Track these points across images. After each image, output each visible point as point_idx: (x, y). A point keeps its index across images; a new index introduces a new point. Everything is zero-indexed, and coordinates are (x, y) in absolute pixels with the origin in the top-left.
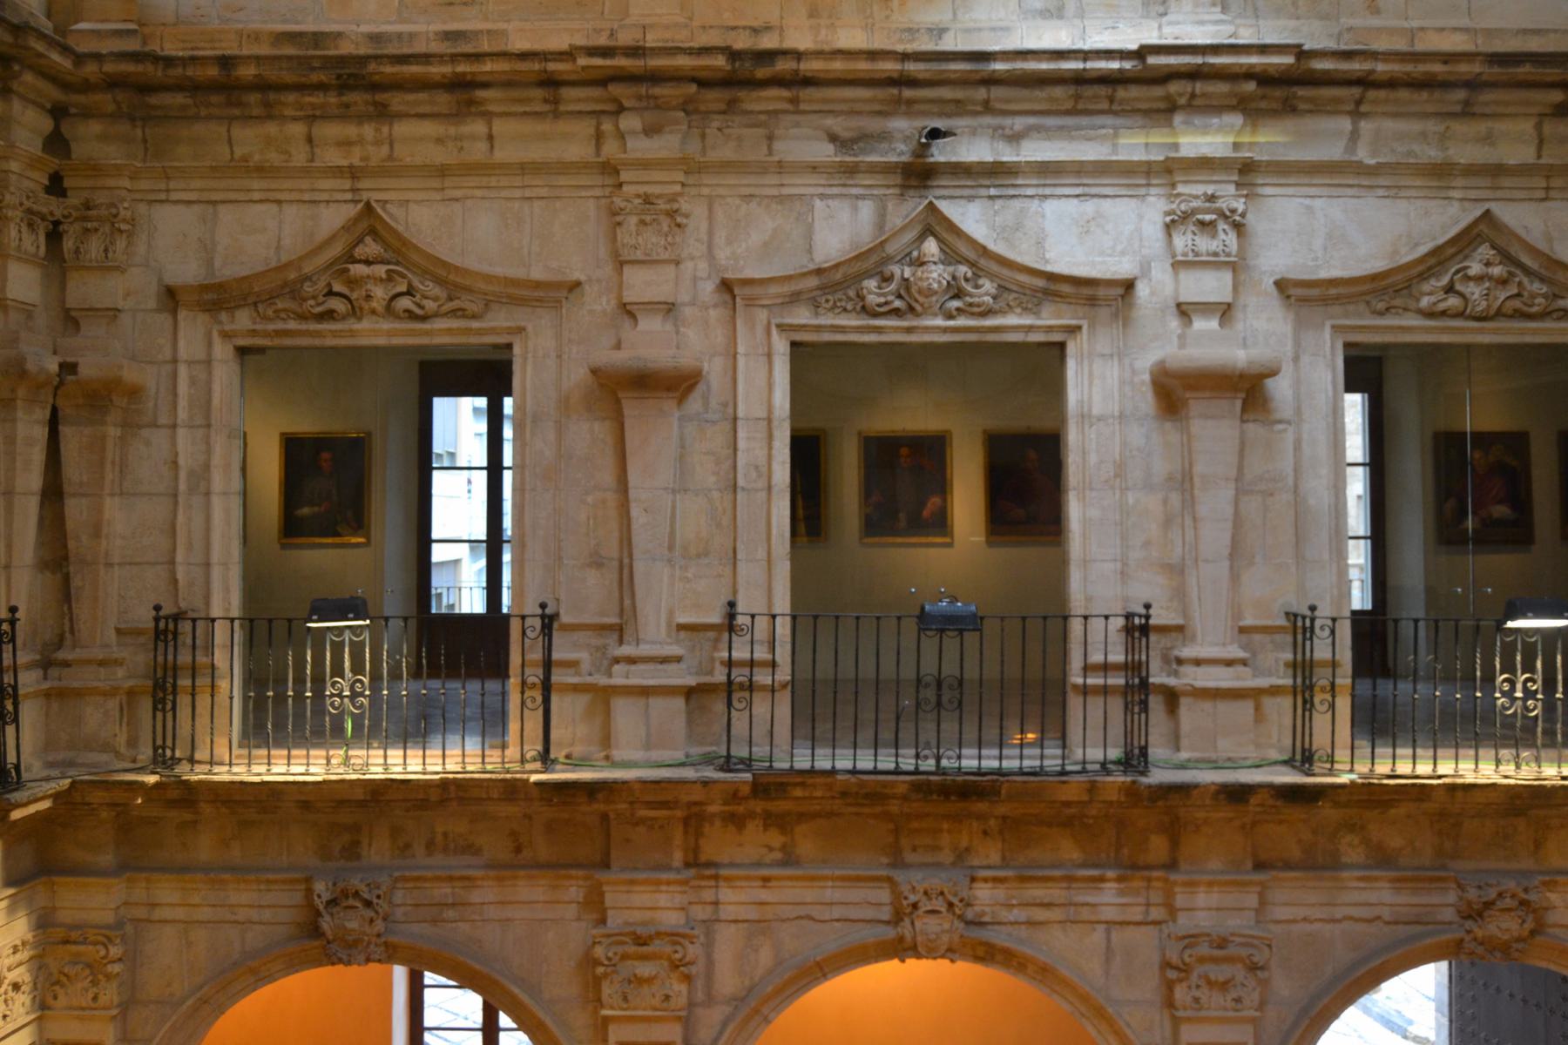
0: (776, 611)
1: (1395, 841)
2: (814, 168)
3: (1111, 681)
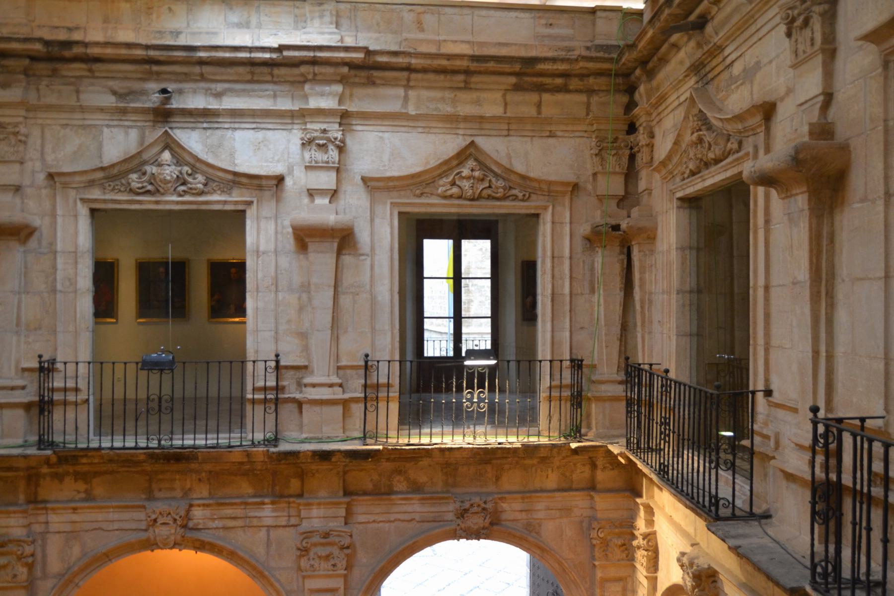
0: (80, 359)
1: (423, 479)
2: (102, 110)
3: (269, 397)
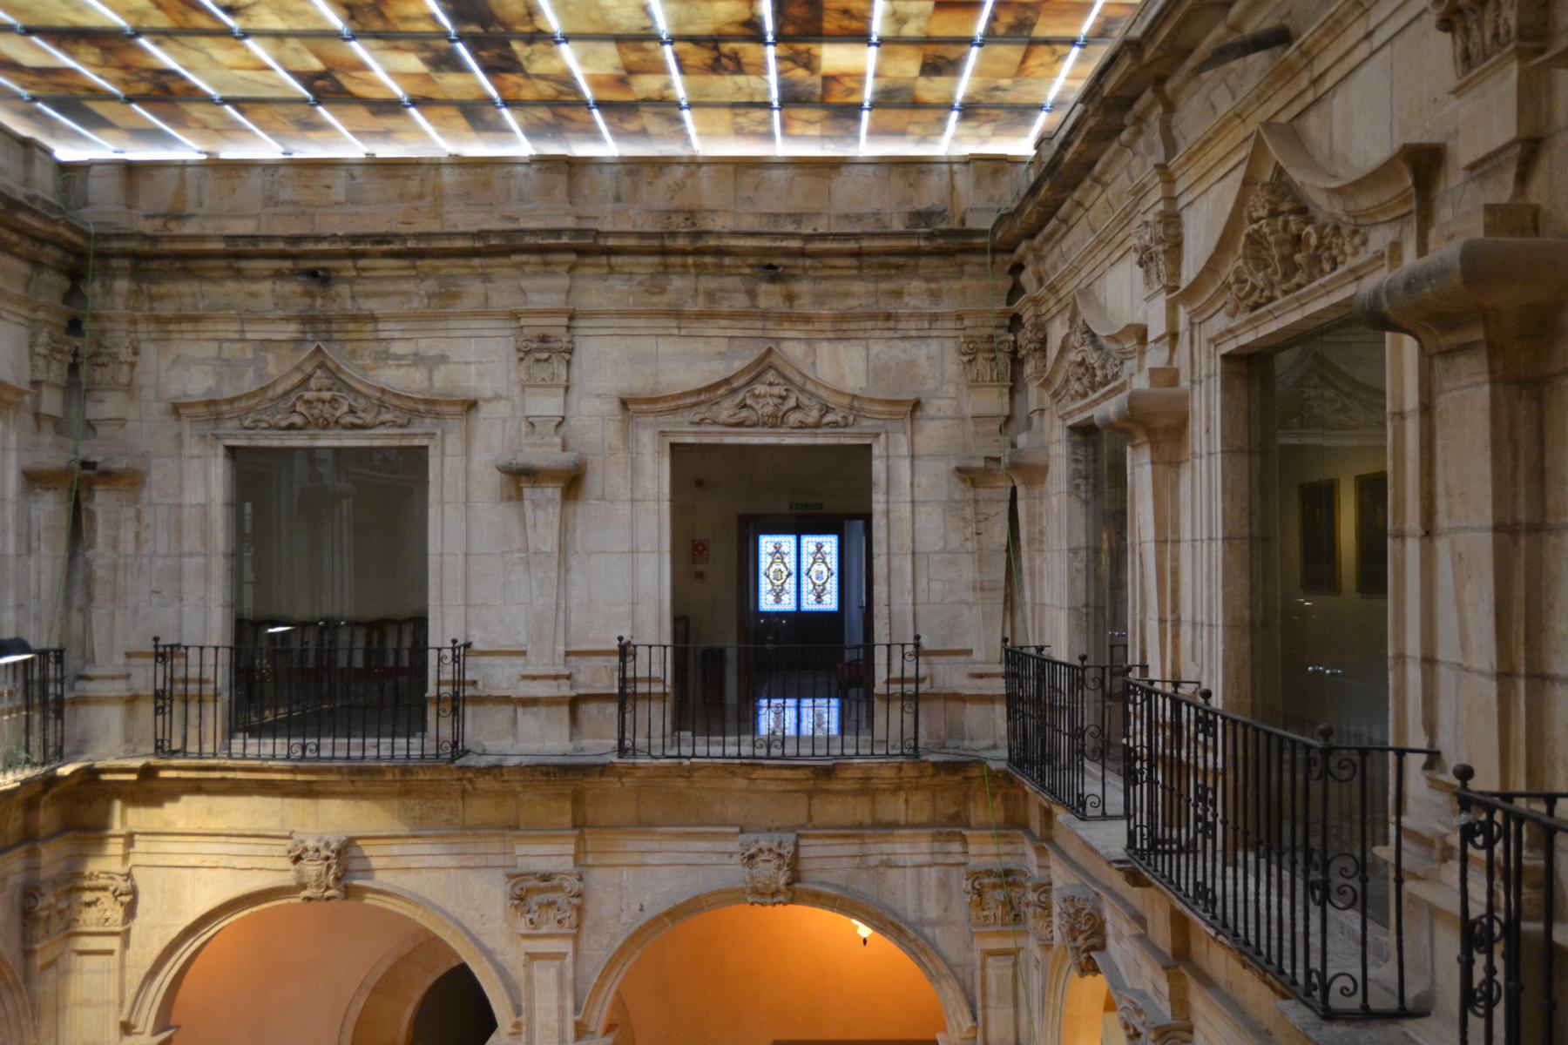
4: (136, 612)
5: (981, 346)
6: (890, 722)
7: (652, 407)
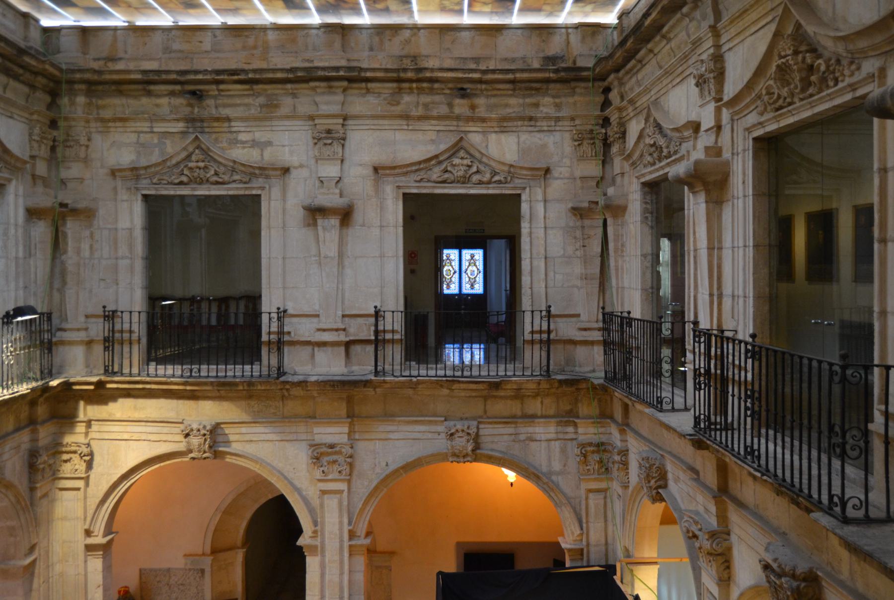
3: (395, 337)
4: (91, 291)
5: (585, 136)
6: (533, 357)
7: (392, 172)
